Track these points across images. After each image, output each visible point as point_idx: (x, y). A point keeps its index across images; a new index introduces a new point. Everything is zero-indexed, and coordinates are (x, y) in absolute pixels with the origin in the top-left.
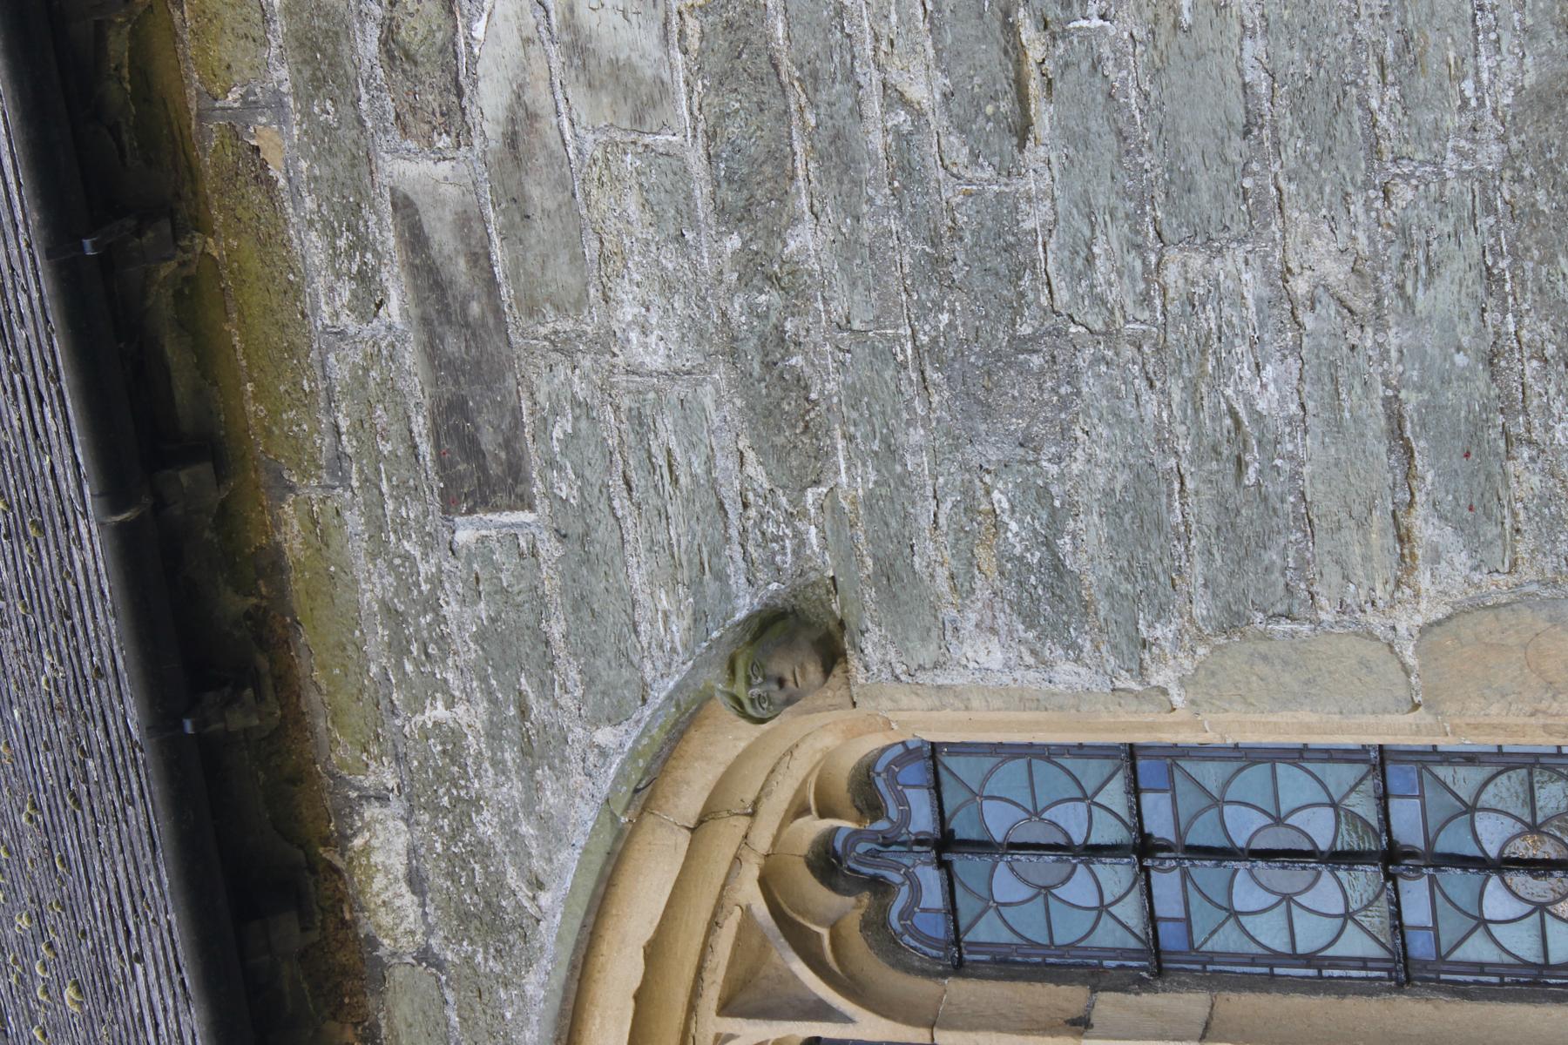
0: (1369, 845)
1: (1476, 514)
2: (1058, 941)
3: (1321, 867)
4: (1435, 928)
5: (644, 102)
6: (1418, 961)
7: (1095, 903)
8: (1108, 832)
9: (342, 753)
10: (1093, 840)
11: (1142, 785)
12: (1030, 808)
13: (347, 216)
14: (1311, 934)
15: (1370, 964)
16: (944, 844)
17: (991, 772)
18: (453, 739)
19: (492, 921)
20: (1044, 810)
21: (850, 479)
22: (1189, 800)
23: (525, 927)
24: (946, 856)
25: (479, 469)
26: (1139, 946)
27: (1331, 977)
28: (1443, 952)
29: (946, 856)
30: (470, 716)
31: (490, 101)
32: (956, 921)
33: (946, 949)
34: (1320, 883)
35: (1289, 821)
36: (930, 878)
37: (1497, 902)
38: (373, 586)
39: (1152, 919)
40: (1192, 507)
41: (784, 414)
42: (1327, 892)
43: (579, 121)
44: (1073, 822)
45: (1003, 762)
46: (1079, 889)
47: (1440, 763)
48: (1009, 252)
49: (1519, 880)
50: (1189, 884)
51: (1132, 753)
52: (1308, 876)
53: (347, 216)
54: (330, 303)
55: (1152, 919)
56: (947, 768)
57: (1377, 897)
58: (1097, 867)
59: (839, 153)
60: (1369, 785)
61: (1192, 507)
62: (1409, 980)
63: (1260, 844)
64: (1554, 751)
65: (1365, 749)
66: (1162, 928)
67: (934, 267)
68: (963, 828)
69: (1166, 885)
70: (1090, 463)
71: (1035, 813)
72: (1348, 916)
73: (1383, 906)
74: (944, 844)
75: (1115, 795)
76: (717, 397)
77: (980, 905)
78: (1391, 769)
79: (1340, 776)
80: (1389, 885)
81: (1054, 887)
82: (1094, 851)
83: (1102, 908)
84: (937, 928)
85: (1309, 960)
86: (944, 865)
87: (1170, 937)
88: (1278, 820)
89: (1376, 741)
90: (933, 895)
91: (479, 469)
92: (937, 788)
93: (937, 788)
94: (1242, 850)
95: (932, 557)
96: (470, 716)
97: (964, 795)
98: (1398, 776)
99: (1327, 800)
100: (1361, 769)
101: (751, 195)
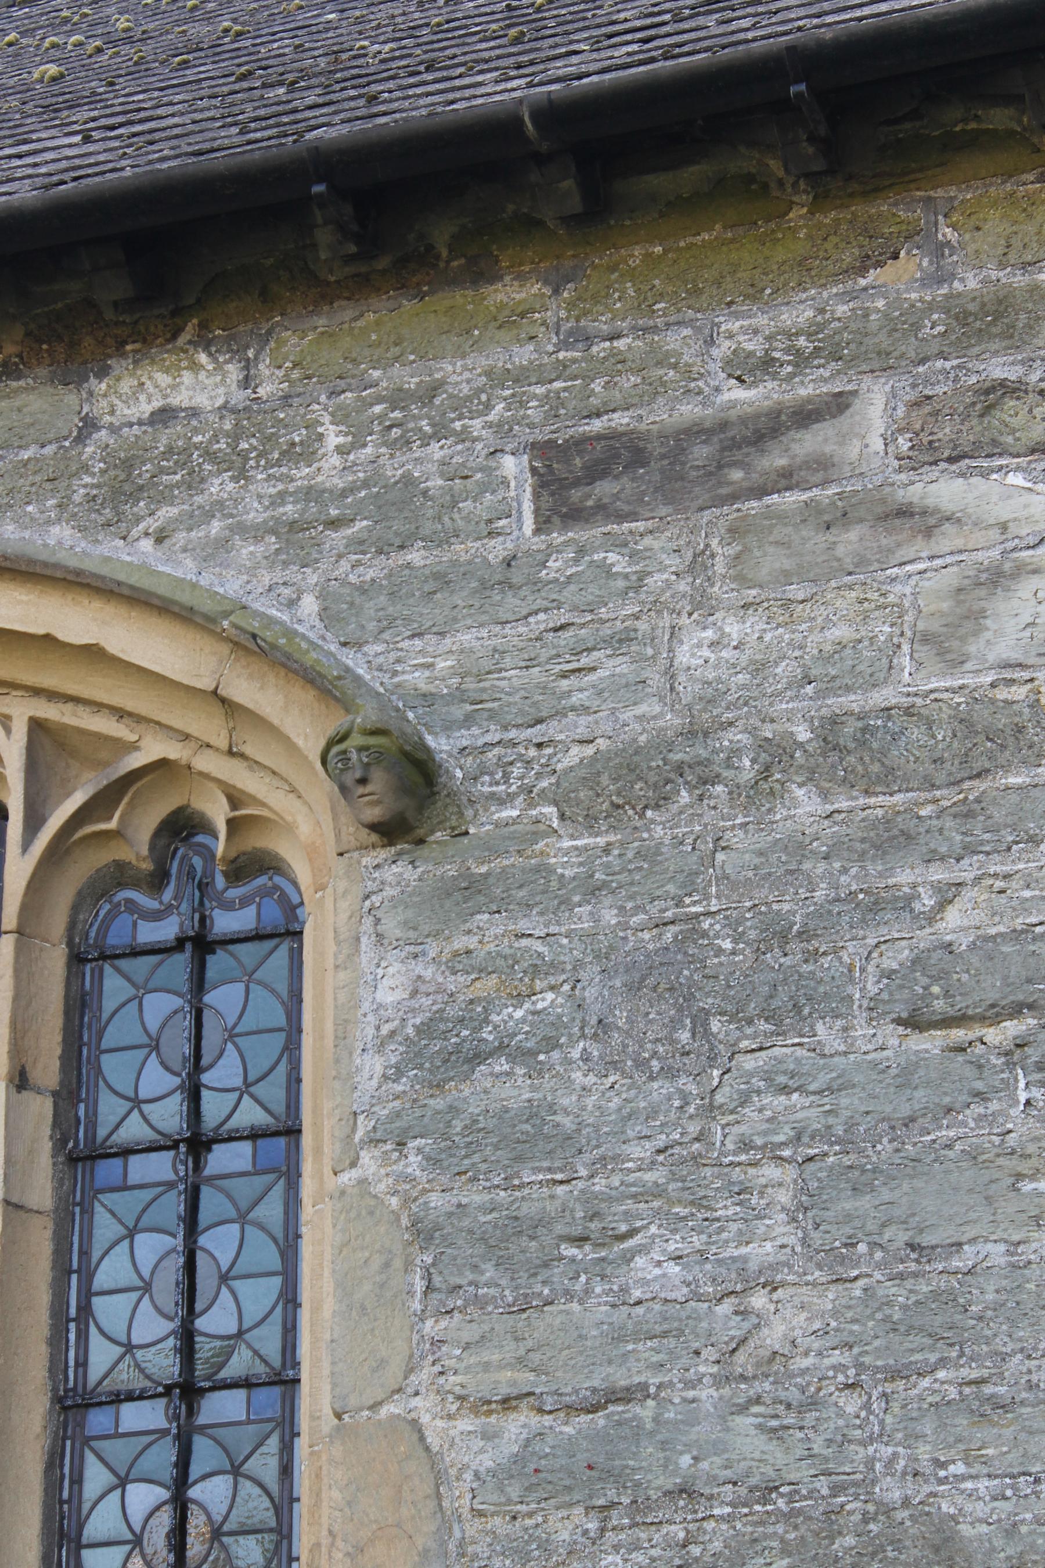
0: (200, 1369)
1: (532, 1476)
2: (104, 1058)
3: (178, 1322)
4: (125, 1188)
5: (943, 644)
6: (84, 1418)
7: (142, 1095)
8: (214, 1108)
9: (293, 342)
10: (205, 1093)
11: (260, 1142)
12: (237, 1030)
13: (828, 347)
14: (110, 1311)
15: (81, 1370)
16: (201, 944)
17: (273, 991)
18: (306, 452)
19: (124, 492)
20: (229, 1287)
21: (566, 850)
22: (245, 1189)
23: (118, 525)
24: (189, 946)
25: (577, 478)
26: (99, 1139)
27: (68, 1331)
28: (93, 1443)
29: (189, 946)
30: (329, 469)
31: (944, 490)
32: (123, 956)
33: (96, 946)
34: (162, 1320)
35: (224, 1289)
36: (167, 930)
37: (143, 1497)
38: (459, 373)
39: (126, 1152)
40: (538, 1193)
41: (632, 784)
42: (153, 1326)
43: (922, 580)
44: (223, 1072)
45: (283, 1003)
46: (156, 1079)
47: (282, 1440)
48: (792, 1008)
49: (165, 1520)
50: (161, 1189)
51: (293, 1132)
52: (170, 1308)
53: (828, 347)
54: (742, 330)
55: (126, 1152)
56: (277, 947)
57: (148, 1377)
58: (177, 1097)
59: (892, 839)
60: (260, 1369)
61: (538, 1193)
62: (65, 1409)
63: (201, 1259)
64: (294, 1554)
65: (296, 1365)
66: (117, 1162)
67: (779, 934)
68: (217, 963)
69: (159, 1167)
70: (581, 1090)
71: (232, 1035)
72: (129, 1348)
73: (140, 1383)
74: (201, 944)
75: (249, 1115)
76: (649, 717)
77: (139, 979)
78: (277, 1390)
79: (273, 1090)
80: (160, 1389)
81: (158, 1054)
82: (194, 1094)
83: (137, 1102)
84: (117, 938)
85: (85, 1310)
86: (179, 945)
87: (108, 1170)
88: (224, 1278)
89: (304, 1376)
90: (150, 933)
91: (577, 478)
92: (257, 937)
93: (257, 937)
94: (195, 1242)
95: (488, 932)
96: (329, 469)
97: (249, 962)
98: (269, 1398)
99: (245, 1326)
100: (276, 1361)
101: (849, 752)
